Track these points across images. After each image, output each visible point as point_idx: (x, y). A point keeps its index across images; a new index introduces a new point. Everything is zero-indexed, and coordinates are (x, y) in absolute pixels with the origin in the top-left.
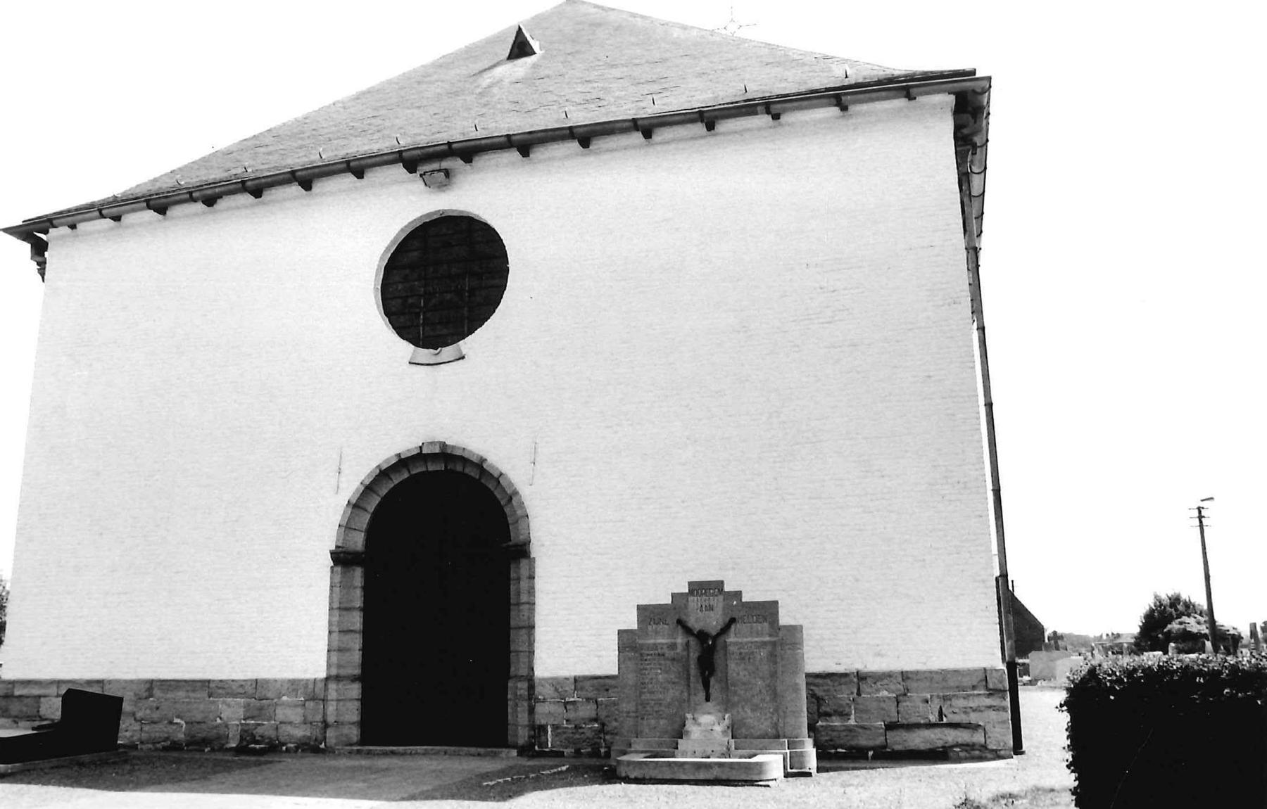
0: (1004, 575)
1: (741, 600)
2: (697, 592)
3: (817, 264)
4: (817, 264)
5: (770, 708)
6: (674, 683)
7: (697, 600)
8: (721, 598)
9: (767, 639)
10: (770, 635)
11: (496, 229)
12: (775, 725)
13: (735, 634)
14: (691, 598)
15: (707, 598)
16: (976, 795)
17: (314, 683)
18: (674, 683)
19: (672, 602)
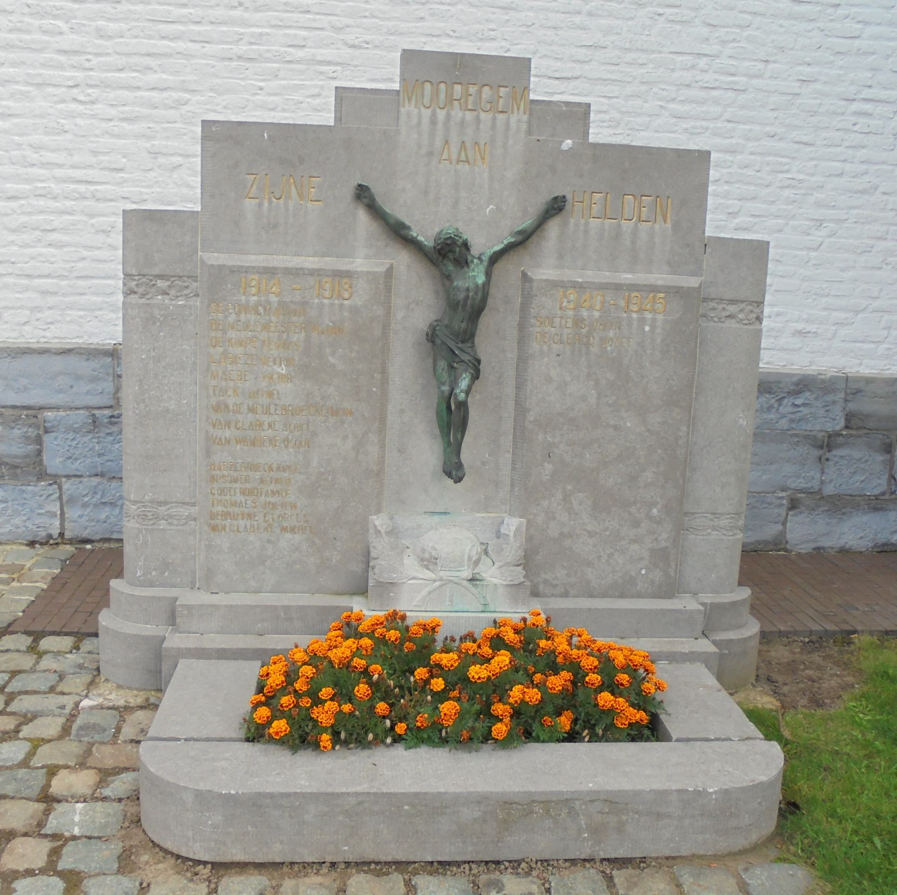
0: (875, 238)
1: (586, 133)
2: (436, 93)
3: (120, 376)
4: (120, 376)
5: (653, 504)
6: (335, 412)
7: (433, 122)
8: (518, 119)
9: (661, 278)
10: (674, 267)
11: (261, 790)
12: (660, 556)
13: (561, 257)
14: (409, 109)
15: (469, 116)
16: (264, 399)
17: (847, 380)
18: (335, 412)
19: (338, 119)
